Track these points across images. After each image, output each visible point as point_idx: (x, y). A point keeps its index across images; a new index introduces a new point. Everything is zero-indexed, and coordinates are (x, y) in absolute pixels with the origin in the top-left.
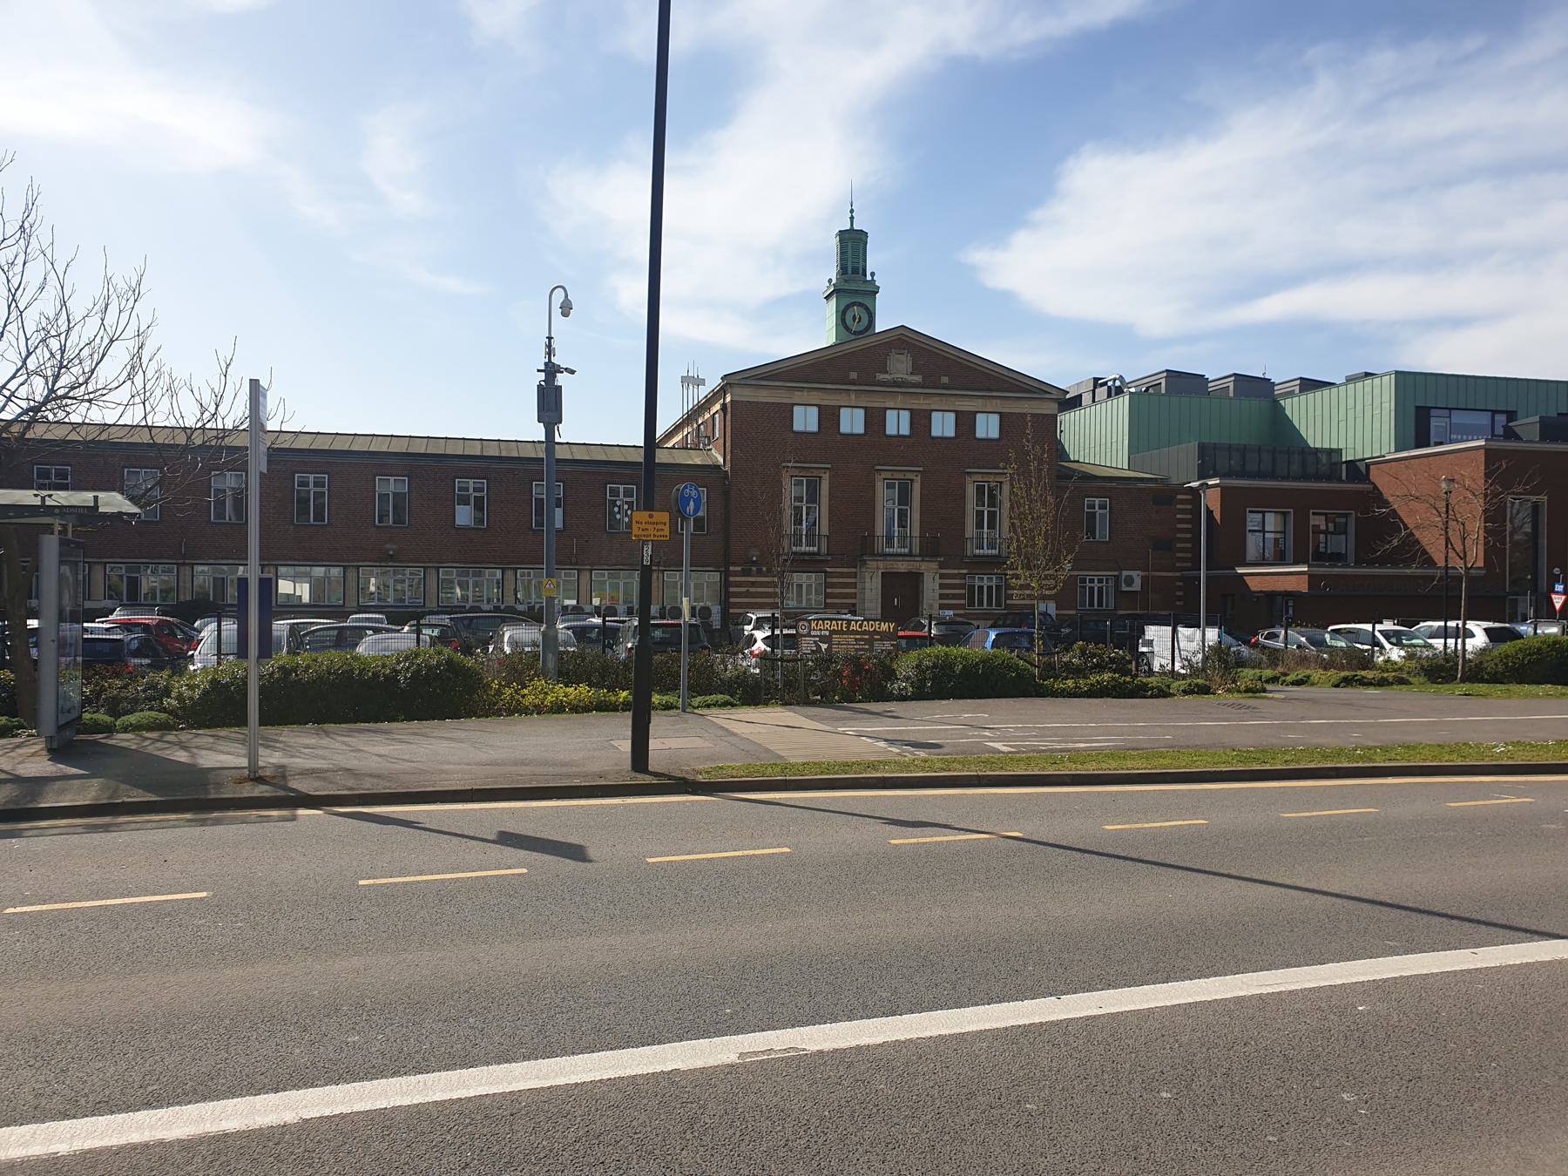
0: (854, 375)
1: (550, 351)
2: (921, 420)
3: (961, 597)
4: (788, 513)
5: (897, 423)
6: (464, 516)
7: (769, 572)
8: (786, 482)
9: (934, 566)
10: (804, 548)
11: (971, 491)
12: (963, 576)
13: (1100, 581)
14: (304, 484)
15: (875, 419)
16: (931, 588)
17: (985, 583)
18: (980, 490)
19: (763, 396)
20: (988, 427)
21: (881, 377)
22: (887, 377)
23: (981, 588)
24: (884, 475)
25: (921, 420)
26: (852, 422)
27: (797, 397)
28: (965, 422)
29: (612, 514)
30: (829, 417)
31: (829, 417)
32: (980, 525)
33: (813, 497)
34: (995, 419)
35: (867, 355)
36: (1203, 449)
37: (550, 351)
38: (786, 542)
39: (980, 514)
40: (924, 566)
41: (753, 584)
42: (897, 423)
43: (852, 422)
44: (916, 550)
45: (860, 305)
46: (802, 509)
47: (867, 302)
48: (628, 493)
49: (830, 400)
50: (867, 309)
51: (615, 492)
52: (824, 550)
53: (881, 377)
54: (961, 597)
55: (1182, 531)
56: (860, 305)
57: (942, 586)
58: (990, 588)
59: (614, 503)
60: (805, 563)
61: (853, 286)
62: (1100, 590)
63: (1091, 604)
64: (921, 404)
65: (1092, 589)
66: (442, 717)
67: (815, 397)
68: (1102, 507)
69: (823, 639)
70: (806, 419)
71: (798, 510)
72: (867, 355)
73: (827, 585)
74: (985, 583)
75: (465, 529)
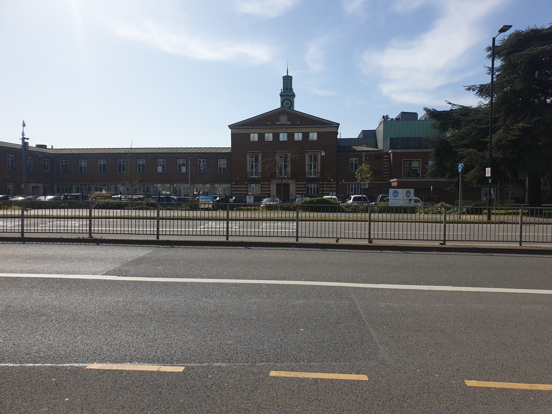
0: (269, 123)
1: (23, 134)
2: (291, 136)
3: (305, 191)
4: (249, 166)
5: (283, 137)
6: (160, 169)
7: (243, 184)
8: (248, 156)
9: (293, 181)
10: (254, 177)
11: (307, 157)
12: (305, 184)
13: (355, 185)
14: (120, 162)
15: (276, 136)
16: (293, 188)
17: (313, 186)
18: (311, 157)
19: (241, 131)
20: (314, 136)
21: (277, 123)
22: (279, 123)
23: (311, 188)
24: (278, 154)
25: (291, 136)
26: (298, 137)
27: (251, 131)
28: (306, 136)
29: (200, 168)
30: (261, 136)
31: (261, 136)
32: (311, 168)
33: (257, 160)
34: (301, 134)
35: (286, 115)
36: (391, 139)
37: (23, 134)
38: (248, 174)
39: (311, 165)
40: (289, 182)
41: (238, 188)
42: (283, 137)
43: (269, 137)
44: (289, 177)
45: (288, 99)
46: (253, 166)
47: (291, 99)
48: (204, 162)
49: (262, 131)
50: (290, 100)
51: (200, 162)
52: (319, 177)
53: (277, 123)
54: (305, 191)
55: (385, 168)
56: (288, 99)
57: (270, 188)
58: (314, 188)
59: (200, 165)
60: (255, 181)
61: (288, 94)
62: (355, 188)
63: (311, 193)
64: (290, 131)
65: (352, 188)
66: (414, 247)
67: (257, 131)
68: (356, 161)
69: (94, 198)
70: (255, 137)
71: (252, 165)
72: (286, 115)
73: (262, 188)
74: (313, 186)
75: (160, 173)
